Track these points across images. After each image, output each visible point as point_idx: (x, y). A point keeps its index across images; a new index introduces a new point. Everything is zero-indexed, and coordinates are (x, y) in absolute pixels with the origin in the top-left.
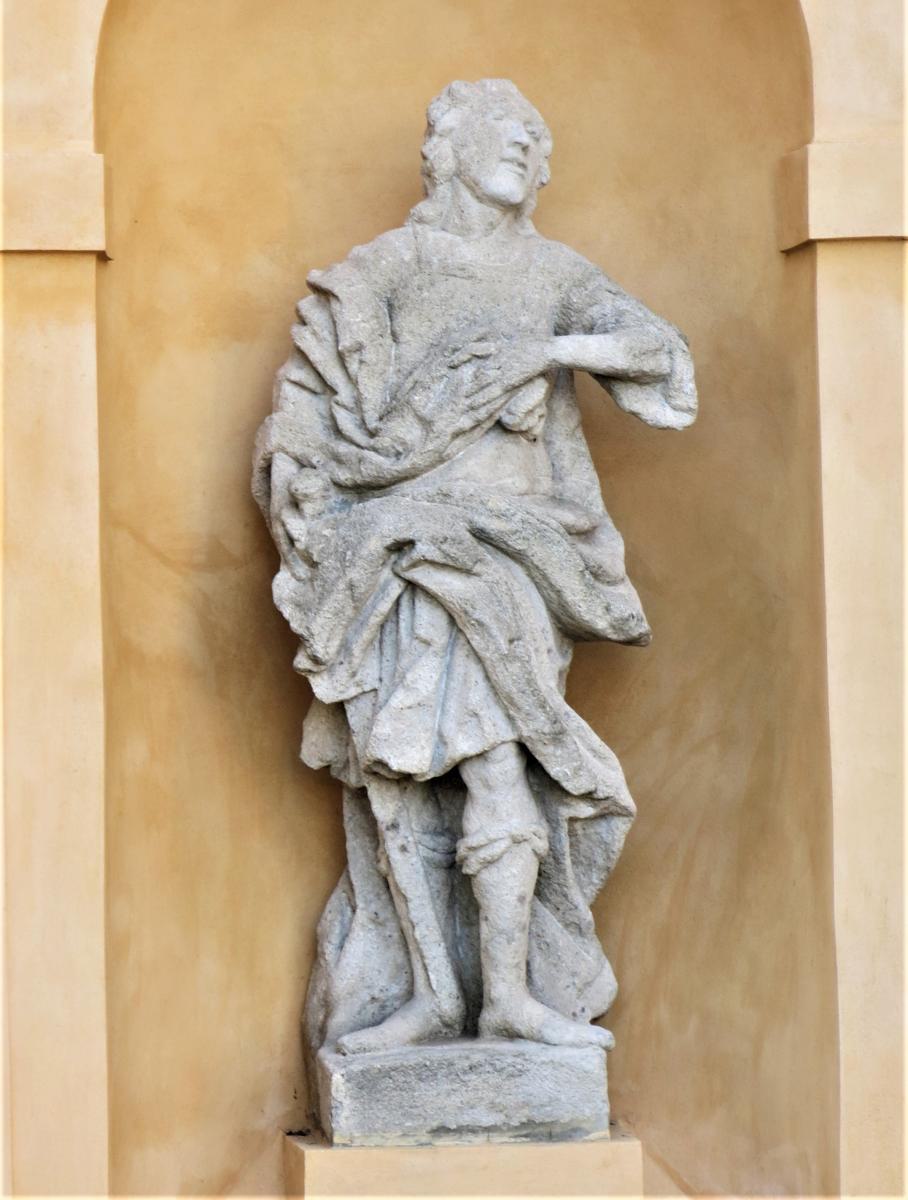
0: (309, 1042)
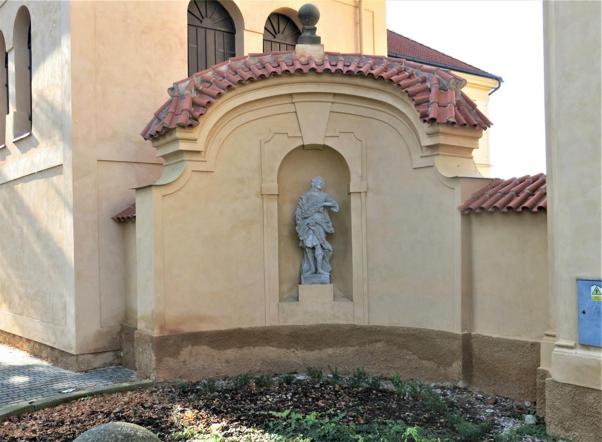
0: (301, 274)
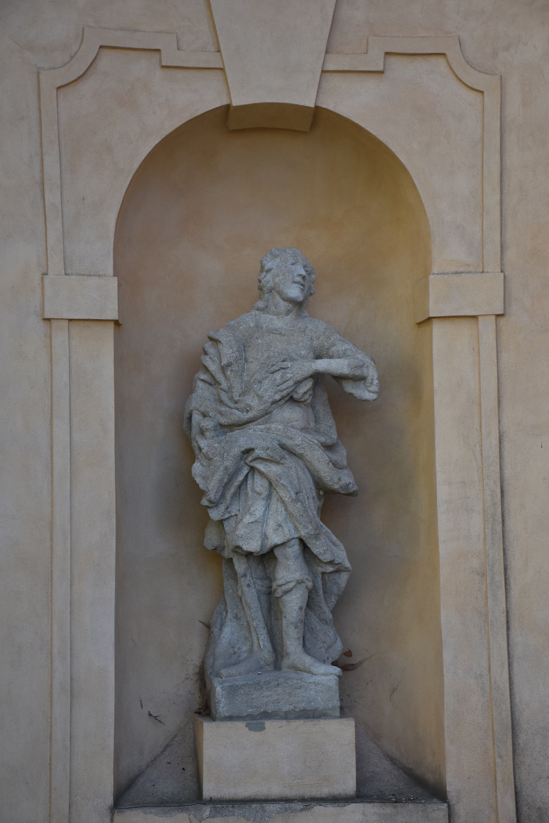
0: (203, 679)
